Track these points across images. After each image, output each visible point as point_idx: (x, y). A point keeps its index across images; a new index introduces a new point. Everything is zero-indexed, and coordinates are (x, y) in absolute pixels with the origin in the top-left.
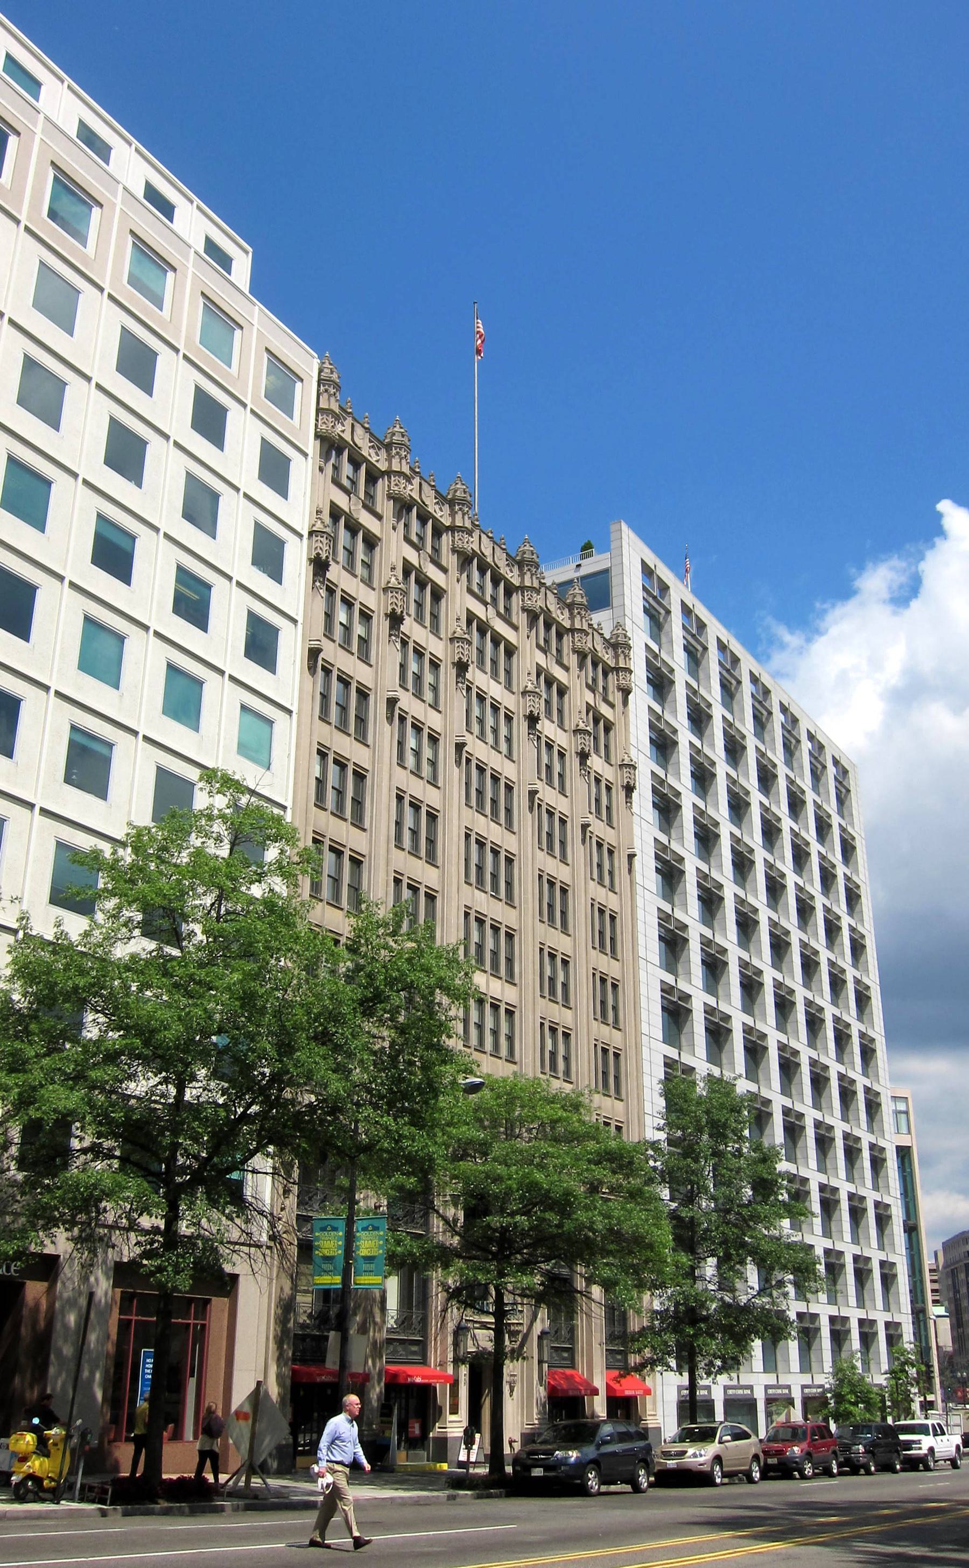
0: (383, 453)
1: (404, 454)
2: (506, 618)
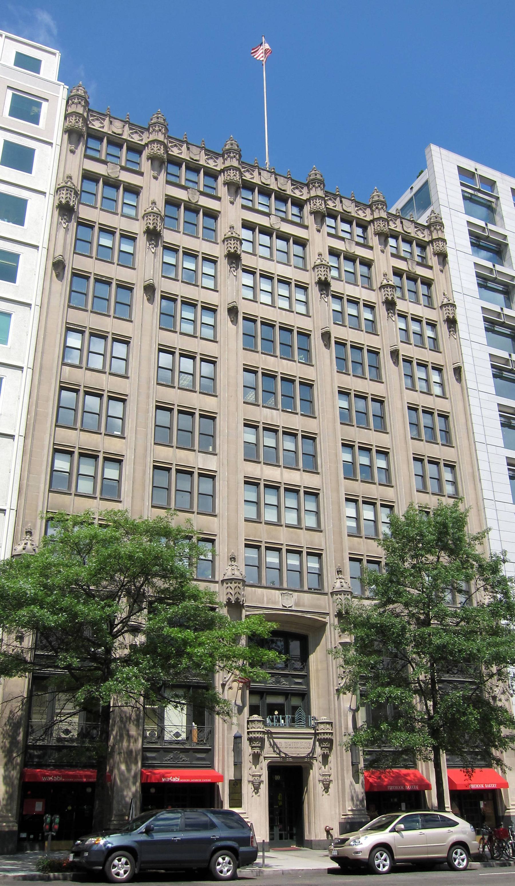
0: (426, 232)
1: (438, 228)
2: (423, 264)
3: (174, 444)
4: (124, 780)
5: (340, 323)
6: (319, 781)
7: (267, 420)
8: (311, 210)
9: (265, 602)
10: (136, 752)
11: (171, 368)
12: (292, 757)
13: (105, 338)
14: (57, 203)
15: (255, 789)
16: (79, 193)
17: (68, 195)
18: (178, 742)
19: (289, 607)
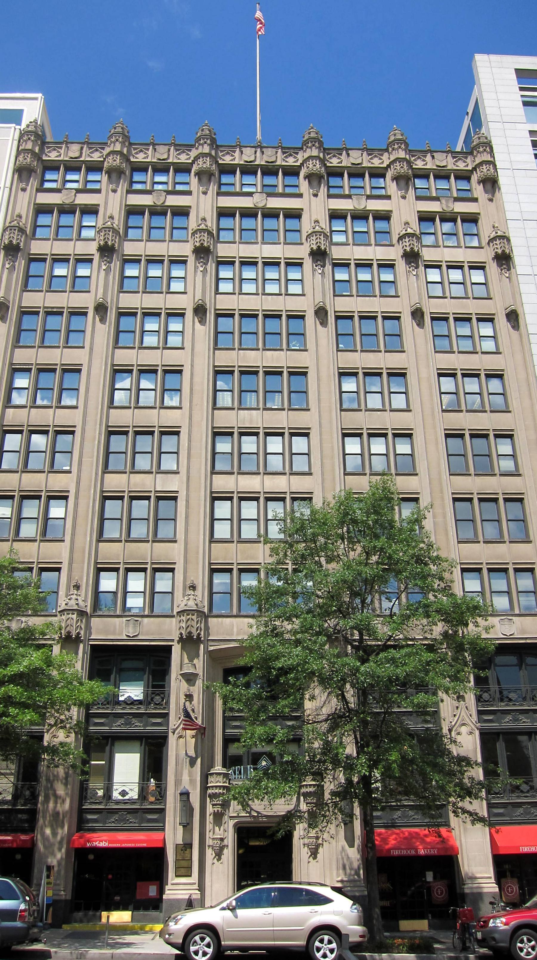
3: (472, 471)
4: (49, 846)
5: (348, 294)
6: (304, 845)
7: (244, 424)
8: (478, 180)
9: (235, 633)
10: (63, 814)
11: (455, 391)
12: (266, 816)
13: (478, 376)
14: (493, 254)
15: (216, 856)
16: (328, 234)
17: (318, 240)
18: (125, 802)
19: (511, 635)
